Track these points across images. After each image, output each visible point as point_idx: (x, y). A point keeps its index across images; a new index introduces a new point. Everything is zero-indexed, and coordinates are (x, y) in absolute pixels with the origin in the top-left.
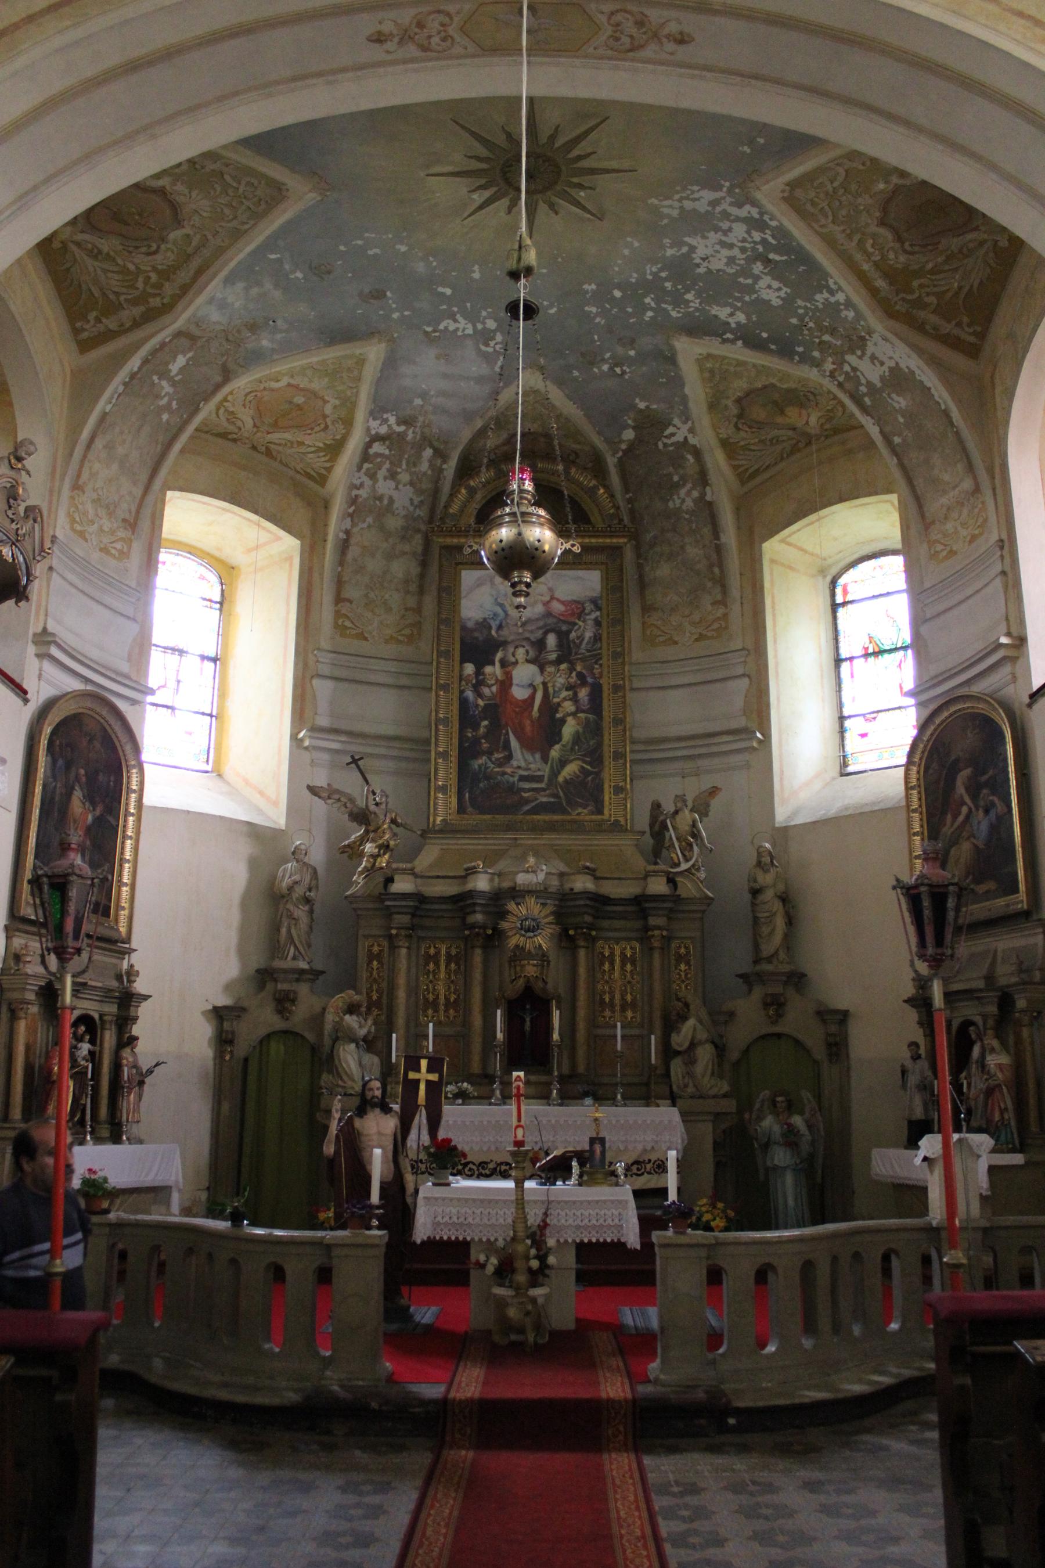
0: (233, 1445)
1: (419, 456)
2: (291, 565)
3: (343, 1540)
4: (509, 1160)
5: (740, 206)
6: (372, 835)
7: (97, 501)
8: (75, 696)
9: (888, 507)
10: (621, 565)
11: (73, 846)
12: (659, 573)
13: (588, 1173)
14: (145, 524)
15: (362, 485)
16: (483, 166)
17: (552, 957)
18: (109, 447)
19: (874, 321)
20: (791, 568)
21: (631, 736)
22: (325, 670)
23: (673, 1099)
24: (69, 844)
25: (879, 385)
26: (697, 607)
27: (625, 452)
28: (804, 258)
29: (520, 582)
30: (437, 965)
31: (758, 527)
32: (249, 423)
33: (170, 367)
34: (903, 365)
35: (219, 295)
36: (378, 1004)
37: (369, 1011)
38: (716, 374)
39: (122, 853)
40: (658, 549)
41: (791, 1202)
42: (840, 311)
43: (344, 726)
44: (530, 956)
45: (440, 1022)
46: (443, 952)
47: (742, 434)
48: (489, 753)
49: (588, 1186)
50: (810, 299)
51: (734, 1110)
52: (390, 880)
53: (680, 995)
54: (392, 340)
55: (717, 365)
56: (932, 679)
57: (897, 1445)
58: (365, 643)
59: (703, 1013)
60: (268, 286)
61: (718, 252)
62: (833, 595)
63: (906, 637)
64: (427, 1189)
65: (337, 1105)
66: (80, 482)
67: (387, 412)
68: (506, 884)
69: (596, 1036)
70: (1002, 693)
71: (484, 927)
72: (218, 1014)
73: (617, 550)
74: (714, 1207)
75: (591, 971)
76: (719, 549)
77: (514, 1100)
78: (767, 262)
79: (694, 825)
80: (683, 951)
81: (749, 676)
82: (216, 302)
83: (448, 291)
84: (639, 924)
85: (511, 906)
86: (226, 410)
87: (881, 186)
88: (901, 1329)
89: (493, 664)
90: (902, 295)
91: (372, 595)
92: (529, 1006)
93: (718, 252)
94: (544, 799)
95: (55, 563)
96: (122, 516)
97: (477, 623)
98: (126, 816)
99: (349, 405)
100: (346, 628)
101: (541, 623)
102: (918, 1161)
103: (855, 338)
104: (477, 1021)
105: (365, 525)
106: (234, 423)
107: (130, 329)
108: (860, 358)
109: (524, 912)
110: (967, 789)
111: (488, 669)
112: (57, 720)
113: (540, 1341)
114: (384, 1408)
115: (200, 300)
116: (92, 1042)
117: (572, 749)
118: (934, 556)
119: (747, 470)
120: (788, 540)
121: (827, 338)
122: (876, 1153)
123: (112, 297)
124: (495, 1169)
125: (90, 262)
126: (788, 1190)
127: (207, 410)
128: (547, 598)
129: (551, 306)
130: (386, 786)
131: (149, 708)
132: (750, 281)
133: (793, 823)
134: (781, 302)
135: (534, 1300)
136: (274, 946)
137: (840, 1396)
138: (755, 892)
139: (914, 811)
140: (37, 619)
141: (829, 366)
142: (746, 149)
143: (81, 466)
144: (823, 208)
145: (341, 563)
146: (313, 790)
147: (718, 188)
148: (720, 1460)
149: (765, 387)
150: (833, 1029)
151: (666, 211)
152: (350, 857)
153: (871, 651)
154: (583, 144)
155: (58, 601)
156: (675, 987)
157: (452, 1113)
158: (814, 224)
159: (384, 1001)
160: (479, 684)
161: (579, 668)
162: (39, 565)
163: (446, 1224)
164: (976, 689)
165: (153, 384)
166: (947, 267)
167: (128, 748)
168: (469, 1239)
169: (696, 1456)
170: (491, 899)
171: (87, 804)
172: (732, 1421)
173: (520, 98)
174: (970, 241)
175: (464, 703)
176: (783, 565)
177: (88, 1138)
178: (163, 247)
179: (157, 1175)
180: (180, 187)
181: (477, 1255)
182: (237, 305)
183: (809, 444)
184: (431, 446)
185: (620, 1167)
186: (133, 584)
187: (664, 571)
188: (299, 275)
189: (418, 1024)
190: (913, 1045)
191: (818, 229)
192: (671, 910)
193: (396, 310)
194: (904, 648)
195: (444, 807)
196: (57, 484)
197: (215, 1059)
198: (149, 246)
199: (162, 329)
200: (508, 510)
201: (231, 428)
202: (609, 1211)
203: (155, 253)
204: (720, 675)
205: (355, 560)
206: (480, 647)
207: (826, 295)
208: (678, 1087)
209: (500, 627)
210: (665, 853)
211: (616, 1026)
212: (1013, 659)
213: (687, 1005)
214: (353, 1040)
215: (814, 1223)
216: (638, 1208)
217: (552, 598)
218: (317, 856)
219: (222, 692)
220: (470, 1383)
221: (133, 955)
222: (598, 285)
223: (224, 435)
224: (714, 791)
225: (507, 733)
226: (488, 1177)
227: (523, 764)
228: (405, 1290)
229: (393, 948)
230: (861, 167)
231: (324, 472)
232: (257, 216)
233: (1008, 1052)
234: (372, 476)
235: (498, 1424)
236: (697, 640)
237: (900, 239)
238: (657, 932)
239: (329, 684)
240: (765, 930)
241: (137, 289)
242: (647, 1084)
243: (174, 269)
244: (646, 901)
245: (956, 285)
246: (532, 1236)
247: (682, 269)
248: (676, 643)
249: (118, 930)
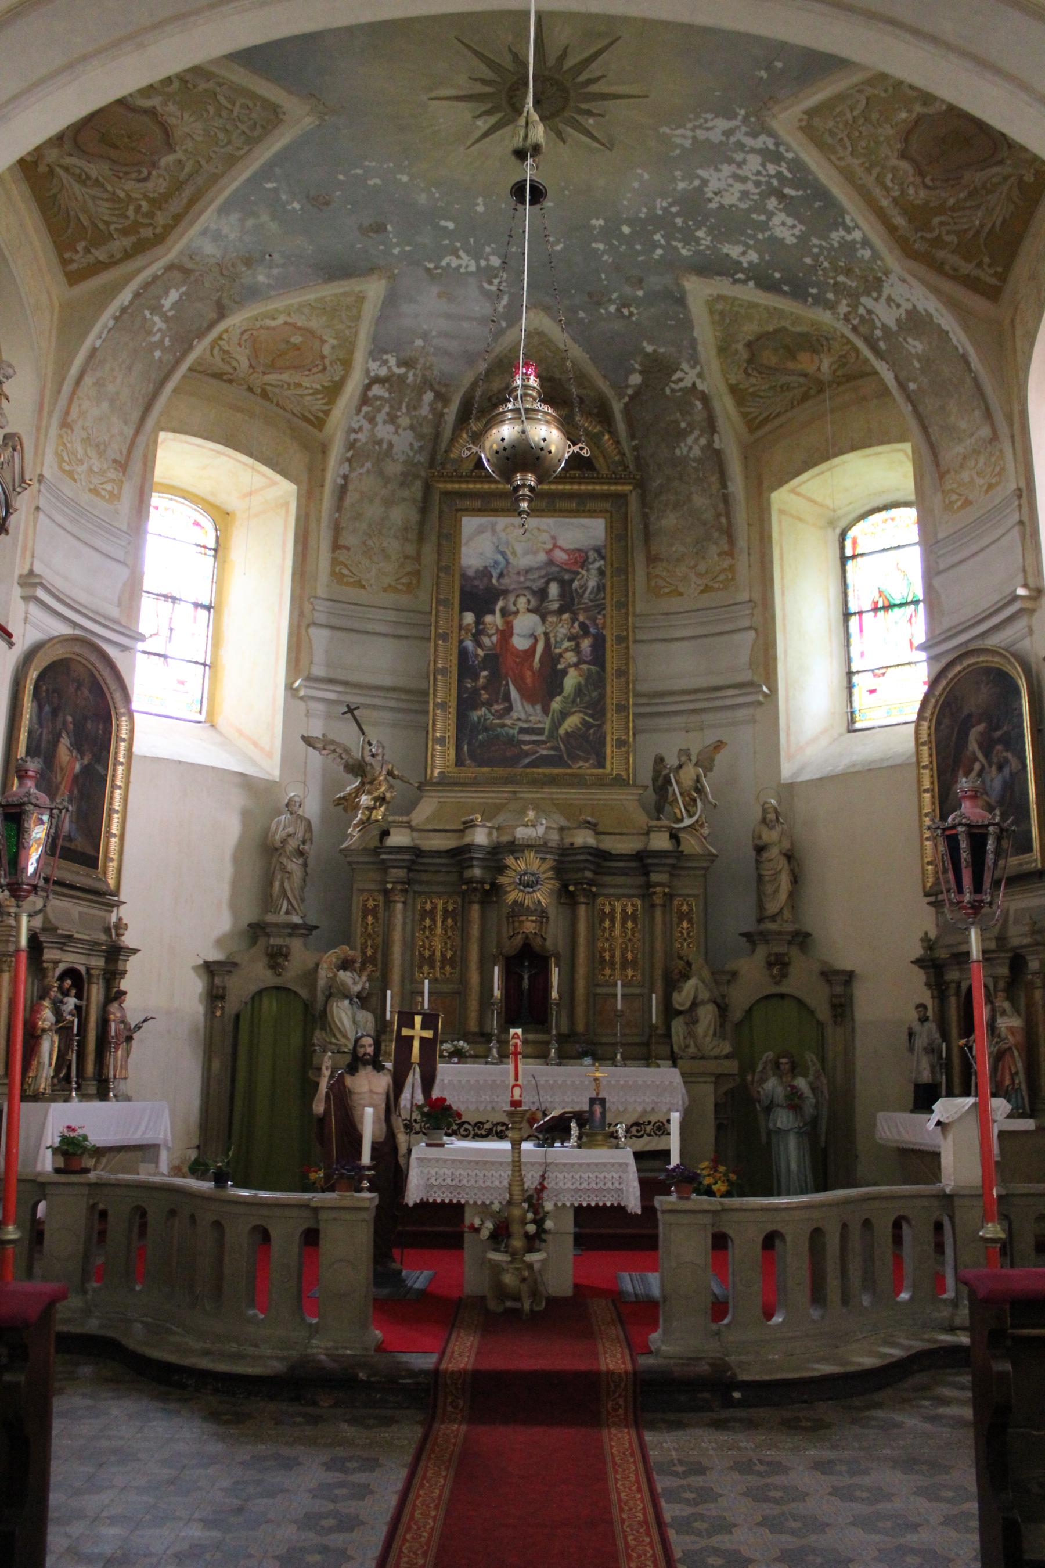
0: (213, 1416)
1: (420, 399)
2: (287, 512)
3: (325, 1523)
4: (506, 1120)
5: (755, 135)
6: (367, 787)
7: (86, 441)
8: (60, 642)
9: (901, 456)
10: (626, 514)
11: (30, 773)
12: (664, 522)
13: (587, 1135)
14: (136, 466)
15: (361, 429)
16: (488, 89)
17: (552, 912)
18: (99, 384)
19: (892, 260)
20: (800, 519)
21: (634, 689)
22: (321, 618)
23: (674, 1060)
24: (26, 771)
25: (894, 328)
26: (704, 558)
27: (632, 398)
28: (822, 193)
29: (524, 485)
30: (434, 920)
31: (762, 484)
32: (244, 363)
33: (163, 301)
34: (920, 308)
35: (213, 226)
36: (372, 960)
37: (363, 968)
38: (726, 315)
39: (111, 804)
40: (663, 498)
41: (793, 1166)
42: (856, 250)
43: (339, 675)
44: (529, 912)
45: (436, 979)
46: (440, 907)
47: (753, 380)
48: (489, 704)
49: (590, 1148)
50: (826, 238)
51: (736, 1072)
52: (385, 833)
53: (682, 953)
54: (392, 278)
55: (728, 307)
56: (945, 632)
57: (910, 1420)
58: (362, 591)
59: (706, 974)
60: (265, 218)
61: (731, 186)
62: (842, 548)
63: (918, 590)
64: (420, 1150)
65: (327, 1062)
66: (69, 419)
67: (386, 353)
68: (505, 838)
69: (596, 995)
70: (1017, 646)
71: (482, 882)
72: (210, 969)
73: (623, 497)
74: (716, 1171)
75: (591, 928)
76: (726, 499)
77: (511, 1060)
78: (782, 197)
79: (698, 780)
80: (685, 908)
81: (756, 630)
82: (210, 233)
83: (451, 225)
84: (640, 880)
85: (510, 861)
86: (221, 349)
87: (903, 115)
88: (912, 1299)
89: (493, 612)
90: (919, 234)
91: (370, 543)
92: (527, 962)
93: (731, 186)
94: (545, 752)
95: (42, 503)
96: (113, 457)
97: (477, 571)
98: (115, 765)
99: (348, 345)
100: (343, 575)
101: (543, 572)
102: (931, 1125)
103: (870, 278)
104: (474, 978)
105: (364, 470)
106: (229, 363)
107: (121, 261)
108: (876, 300)
109: (523, 867)
110: (981, 745)
111: (488, 618)
112: (45, 664)
113: (537, 1309)
114: (373, 1379)
115: (193, 231)
116: (79, 996)
117: (574, 701)
118: (948, 507)
119: (756, 418)
120: (799, 490)
121: (841, 279)
122: (881, 1115)
123: (101, 225)
124: (491, 1129)
125: (77, 187)
126: (791, 1155)
127: (200, 348)
128: (549, 546)
129: (558, 242)
130: (383, 739)
131: (139, 656)
132: (763, 218)
133: (799, 780)
134: (795, 241)
135: (530, 1266)
136: (267, 901)
137: (850, 1369)
138: (760, 849)
139: (924, 767)
140: (23, 556)
141: (843, 308)
142: (763, 74)
143: (71, 400)
144: (841, 139)
145: (339, 508)
146: (308, 741)
147: (733, 116)
148: (724, 1437)
149: (776, 331)
150: (839, 989)
151: (678, 141)
152: (345, 810)
153: (880, 605)
154: (594, 65)
155: (47, 540)
156: (677, 945)
157: (447, 1073)
158: (833, 157)
159: (379, 956)
160: (478, 634)
161: (581, 618)
162: (19, 497)
163: (440, 1186)
164: (992, 642)
165: (145, 318)
166: (968, 204)
167: (118, 696)
168: (463, 1201)
169: (699, 1432)
170: (488, 853)
171: (75, 753)
172: (737, 1395)
173: (527, 13)
174: (993, 176)
175: (463, 654)
176: (792, 516)
177: (74, 1094)
178: (154, 173)
179: (144, 1133)
180: (172, 108)
181: (472, 1219)
182: (232, 236)
183: (821, 391)
184: (432, 389)
185: (621, 1129)
186: (124, 528)
187: (670, 520)
188: (297, 206)
189: (413, 981)
190: (922, 1006)
191: (838, 163)
192: (673, 866)
193: (397, 245)
194: (916, 602)
195: (442, 759)
196: (44, 422)
197: (206, 1015)
198: (140, 172)
199: (153, 262)
200: (510, 406)
201: (227, 369)
202: (609, 1175)
203: (145, 180)
204: (727, 628)
205: (352, 505)
206: (480, 596)
207: (842, 233)
208: (680, 1047)
209: (501, 575)
210: (667, 807)
211: (616, 985)
212: (1032, 611)
213: (689, 964)
214: (347, 996)
215: (818, 1189)
216: (639, 1170)
217: (555, 546)
218: (312, 808)
219: (216, 641)
220: (463, 1353)
221: (122, 908)
222: (605, 220)
223: (218, 376)
224: (719, 745)
225: (507, 684)
226: (484, 1137)
227: (523, 716)
228: (396, 1252)
229: (389, 903)
230: (883, 95)
231: (321, 415)
232: (252, 141)
233: (1019, 1014)
234: (372, 420)
235: (492, 1396)
236: (702, 592)
237: (921, 174)
238: (658, 889)
239: (325, 633)
240: (769, 889)
241: (128, 217)
242: (647, 1044)
243: (166, 197)
244: (649, 857)
245: (977, 222)
246: (529, 1199)
247: (693, 204)
248: (681, 594)
249: (106, 882)
